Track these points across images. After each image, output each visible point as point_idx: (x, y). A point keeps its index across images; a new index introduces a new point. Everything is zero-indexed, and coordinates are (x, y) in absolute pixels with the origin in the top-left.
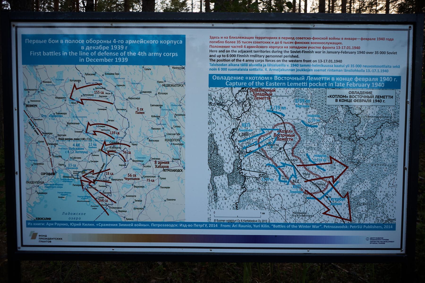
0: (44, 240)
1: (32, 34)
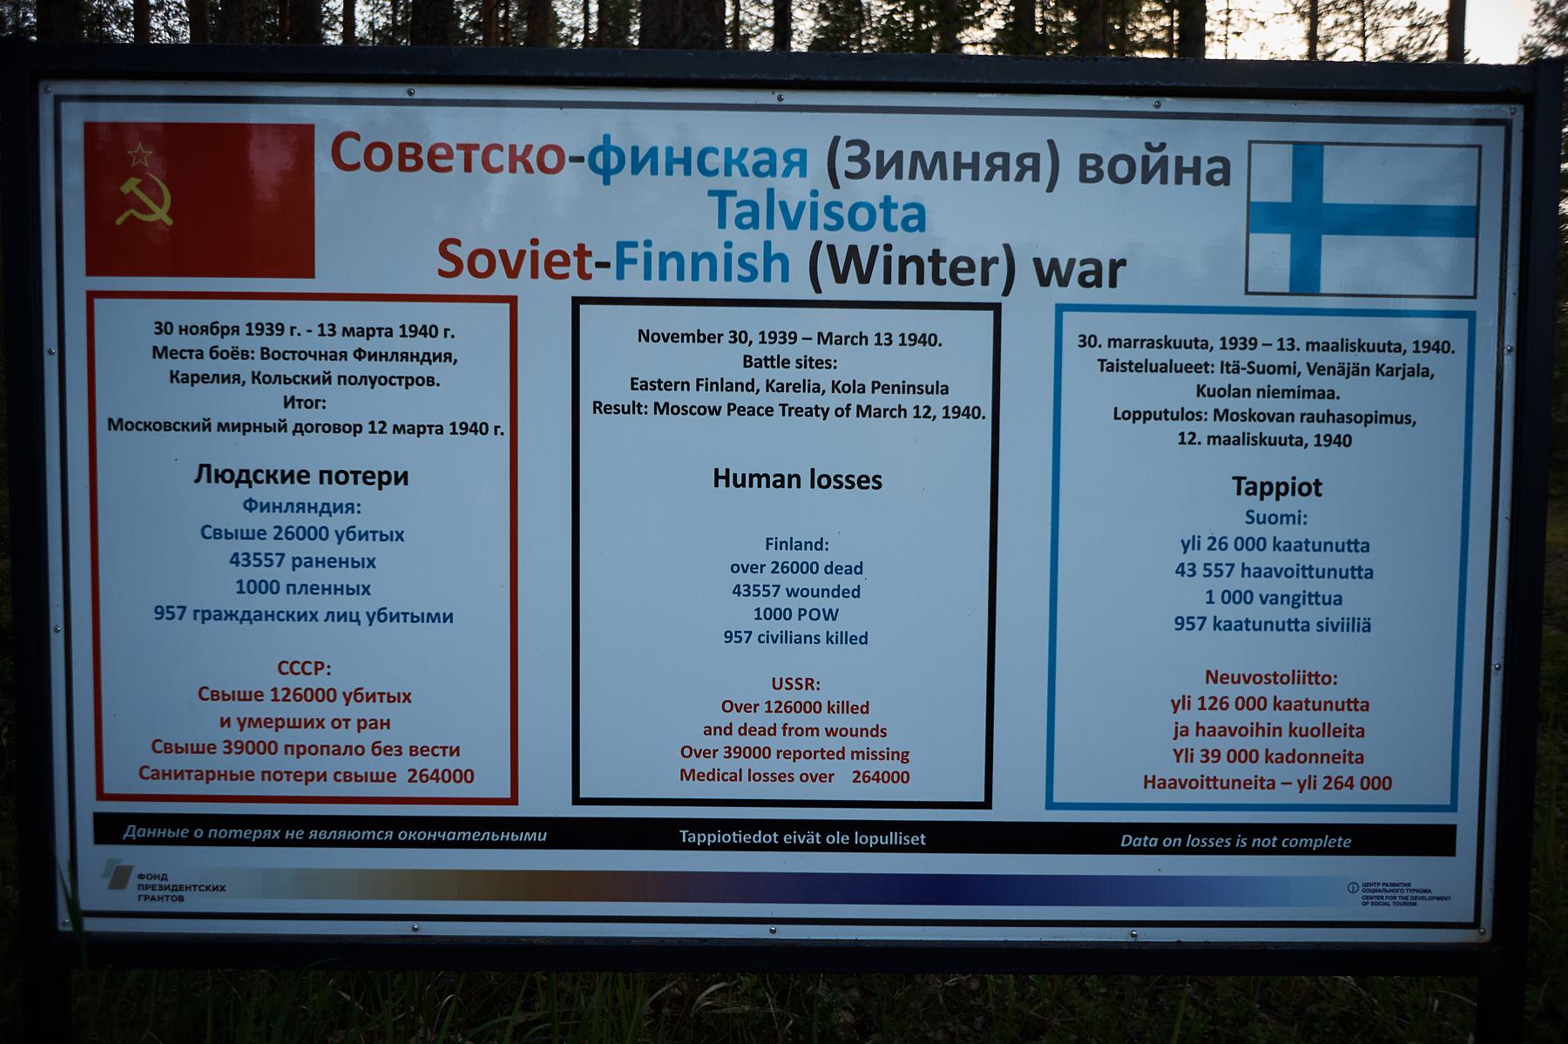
0: (157, 893)
1: (1380, 202)
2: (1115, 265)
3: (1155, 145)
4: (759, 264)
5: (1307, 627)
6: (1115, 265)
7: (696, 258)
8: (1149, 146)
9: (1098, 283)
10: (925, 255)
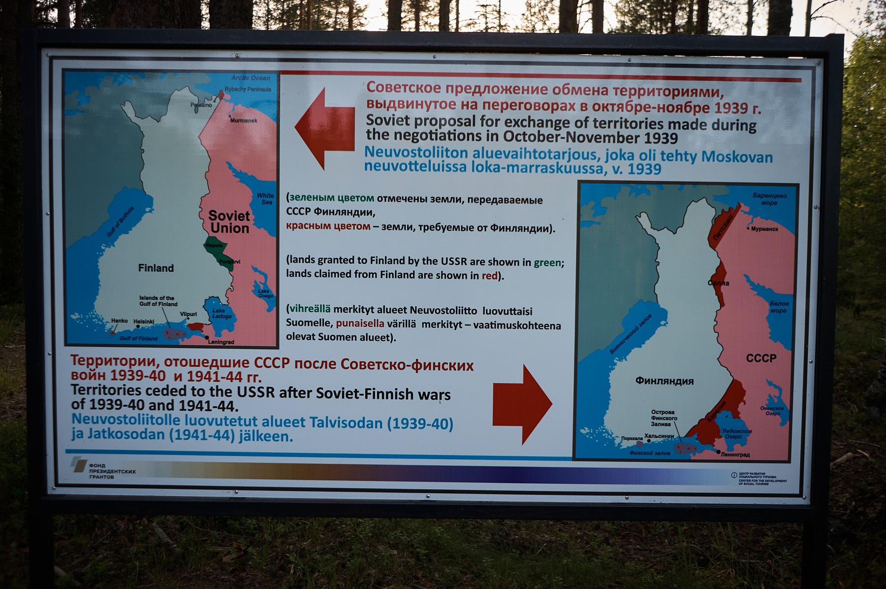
0: (99, 474)
4: (405, 394)
7: (387, 393)
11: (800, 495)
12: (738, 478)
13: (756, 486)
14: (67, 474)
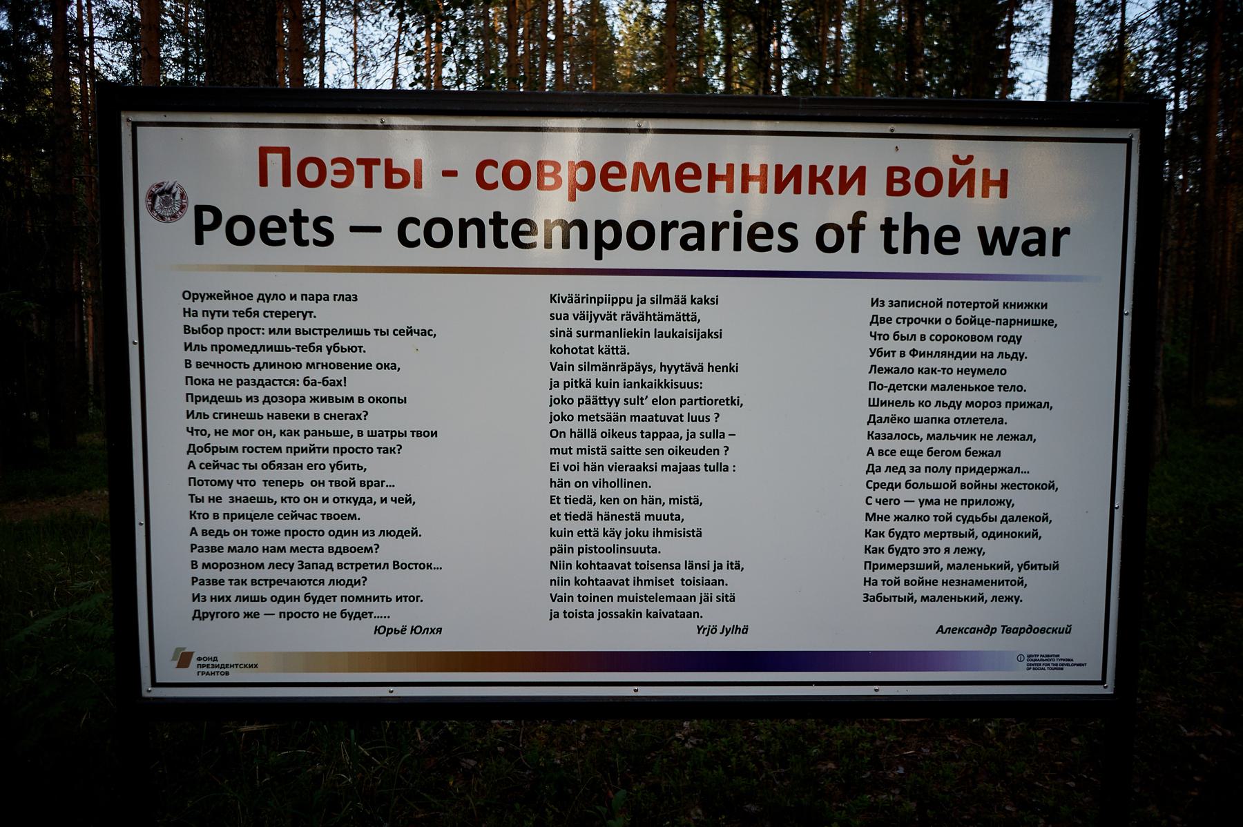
0: (210, 670)
2: (1059, 234)
3: (963, 158)
5: (592, 615)
6: (1059, 234)
8: (956, 159)
9: (700, 246)
10: (486, 218)
11: (1103, 682)
12: (1026, 662)
13: (1047, 671)
14: (167, 670)
